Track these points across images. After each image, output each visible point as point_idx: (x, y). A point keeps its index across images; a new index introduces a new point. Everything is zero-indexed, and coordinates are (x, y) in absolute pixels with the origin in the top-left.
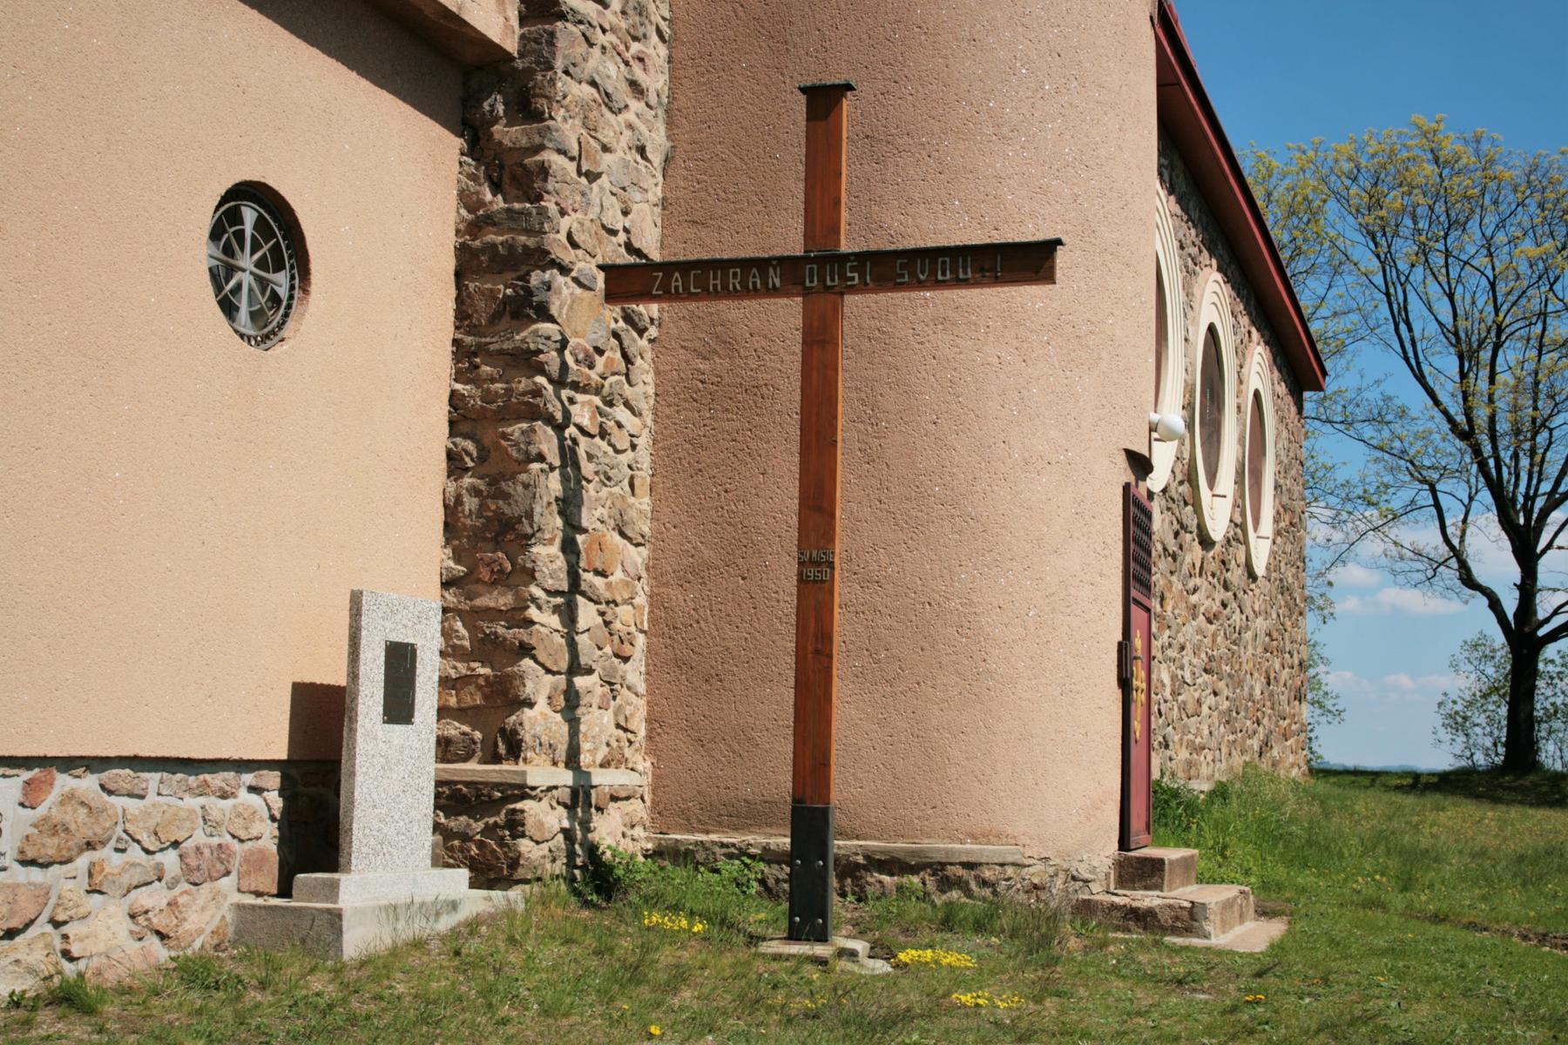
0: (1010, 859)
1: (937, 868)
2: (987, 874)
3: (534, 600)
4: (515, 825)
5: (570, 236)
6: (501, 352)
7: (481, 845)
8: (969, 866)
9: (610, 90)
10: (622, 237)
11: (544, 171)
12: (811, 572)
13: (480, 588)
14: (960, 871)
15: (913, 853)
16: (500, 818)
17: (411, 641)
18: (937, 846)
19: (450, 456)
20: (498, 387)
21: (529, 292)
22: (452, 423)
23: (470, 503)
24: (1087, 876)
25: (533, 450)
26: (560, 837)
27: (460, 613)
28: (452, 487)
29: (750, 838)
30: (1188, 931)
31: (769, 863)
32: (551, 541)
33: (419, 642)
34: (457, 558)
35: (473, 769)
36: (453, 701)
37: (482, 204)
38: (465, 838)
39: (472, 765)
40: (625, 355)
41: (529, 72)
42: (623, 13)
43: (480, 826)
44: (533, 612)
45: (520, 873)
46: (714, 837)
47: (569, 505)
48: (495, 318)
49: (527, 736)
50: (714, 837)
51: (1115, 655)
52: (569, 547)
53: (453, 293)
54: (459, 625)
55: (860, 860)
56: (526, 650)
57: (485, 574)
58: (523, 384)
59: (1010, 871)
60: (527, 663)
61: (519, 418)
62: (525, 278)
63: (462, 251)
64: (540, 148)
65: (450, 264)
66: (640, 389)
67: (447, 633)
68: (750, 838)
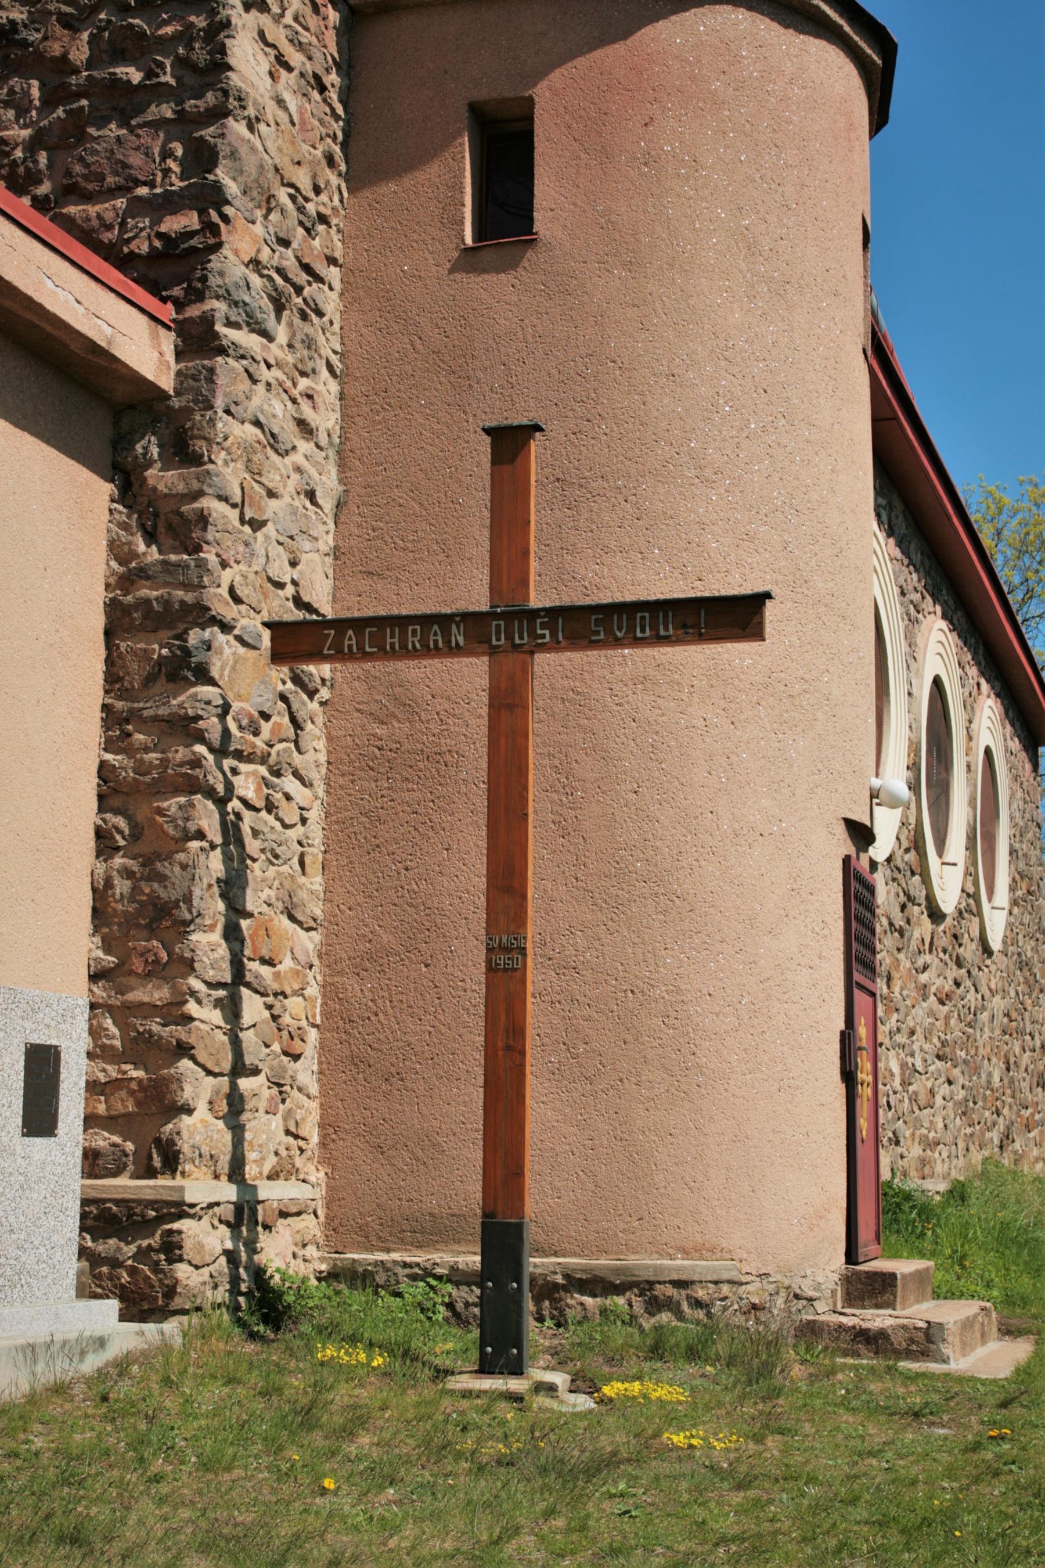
0: (725, 1276)
1: (645, 1287)
2: (700, 1293)
3: (193, 993)
4: (172, 1248)
5: (232, 590)
6: (156, 719)
7: (133, 1271)
8: (680, 1284)
9: (276, 431)
10: (290, 590)
11: (203, 519)
12: (501, 959)
13: (133, 981)
14: (670, 1291)
15: (617, 1271)
16: (155, 1241)
17: (54, 1042)
18: (644, 1262)
19: (100, 834)
20: (153, 756)
21: (187, 653)
22: (101, 797)
23: (122, 886)
24: (811, 1293)
25: (192, 827)
26: (223, 1260)
27: (110, 1009)
28: (101, 868)
29: (436, 1257)
30: (924, 1354)
31: (457, 1284)
32: (212, 928)
33: (63, 1044)
34: (107, 946)
35: (125, 1185)
36: (101, 1109)
37: (134, 555)
38: (115, 1263)
39: (123, 1181)
40: (293, 720)
41: (187, 412)
42: (290, 346)
43: (131, 1250)
44: (191, 1007)
45: (178, 1303)
46: (396, 1256)
47: (232, 888)
48: (149, 680)
49: (185, 1146)
50: (396, 1256)
51: (836, 1046)
52: (232, 934)
53: (102, 653)
54: (109, 1023)
55: (559, 1279)
56: (184, 1050)
57: (138, 965)
58: (181, 754)
59: (725, 1289)
60: (185, 1064)
61: (177, 791)
62: (182, 636)
63: (112, 607)
64: (200, 494)
65: (98, 621)
66: (310, 756)
67: (94, 1032)
68: (436, 1257)
